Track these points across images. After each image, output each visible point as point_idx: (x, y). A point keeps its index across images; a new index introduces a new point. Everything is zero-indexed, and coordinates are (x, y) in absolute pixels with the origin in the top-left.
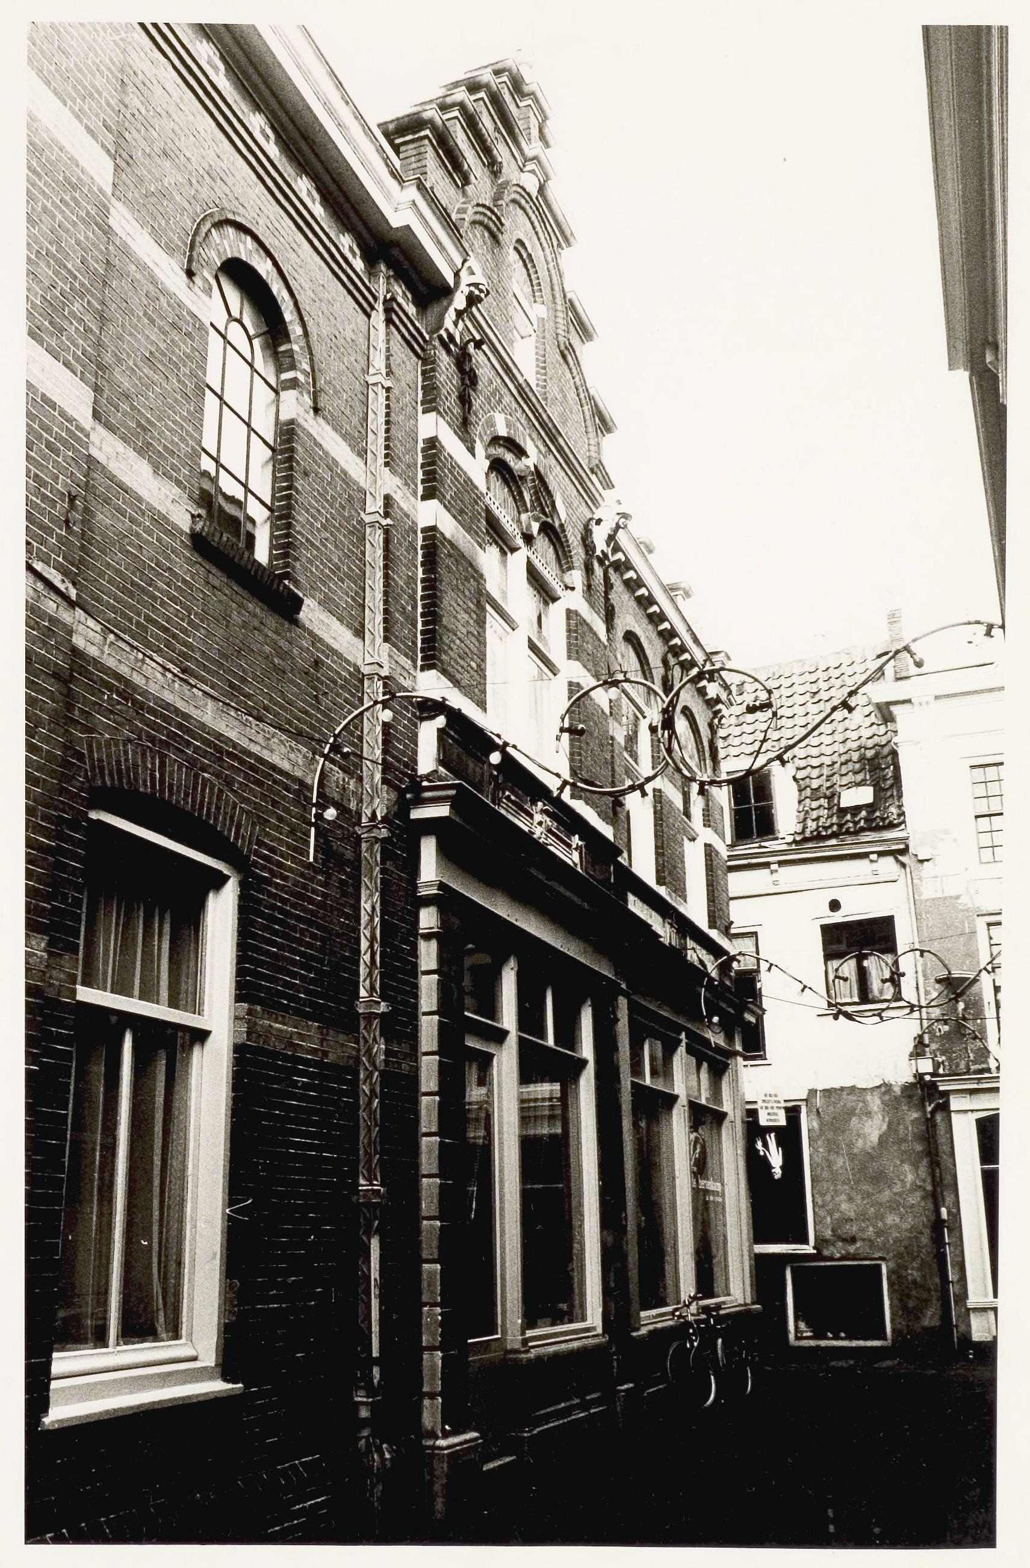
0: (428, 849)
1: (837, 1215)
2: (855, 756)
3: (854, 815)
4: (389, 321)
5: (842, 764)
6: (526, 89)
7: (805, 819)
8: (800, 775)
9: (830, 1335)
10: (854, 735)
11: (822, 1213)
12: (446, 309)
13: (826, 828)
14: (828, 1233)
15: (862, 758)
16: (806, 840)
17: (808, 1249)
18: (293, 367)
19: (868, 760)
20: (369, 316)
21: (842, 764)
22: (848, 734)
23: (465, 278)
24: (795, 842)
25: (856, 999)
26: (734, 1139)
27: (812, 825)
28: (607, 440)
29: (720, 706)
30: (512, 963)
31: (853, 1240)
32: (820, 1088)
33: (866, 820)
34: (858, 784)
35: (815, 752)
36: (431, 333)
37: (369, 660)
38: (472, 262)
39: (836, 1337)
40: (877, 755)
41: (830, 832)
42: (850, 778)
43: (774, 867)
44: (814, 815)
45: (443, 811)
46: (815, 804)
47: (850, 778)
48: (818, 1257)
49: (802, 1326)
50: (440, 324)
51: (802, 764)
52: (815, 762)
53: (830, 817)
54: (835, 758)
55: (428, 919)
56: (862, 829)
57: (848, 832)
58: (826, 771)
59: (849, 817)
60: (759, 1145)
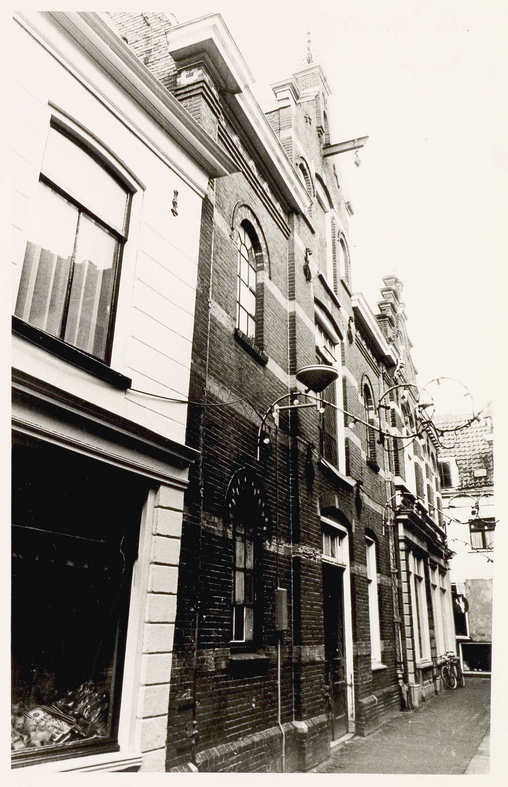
0: (401, 526)
1: (477, 626)
2: (478, 456)
3: (480, 480)
4: (384, 379)
5: (474, 459)
6: (399, 281)
7: (462, 481)
8: (459, 462)
9: (476, 670)
10: (477, 448)
11: (472, 624)
12: (394, 371)
13: (470, 485)
14: (474, 632)
15: (481, 458)
16: (463, 489)
17: (467, 638)
18: (372, 404)
19: (483, 458)
20: (378, 378)
21: (474, 459)
22: (475, 447)
23: (400, 362)
24: (459, 489)
25: (482, 547)
26: (448, 598)
27: (465, 483)
28: (416, 375)
29: (439, 448)
30: (411, 553)
31: (484, 635)
32: (470, 579)
33: (485, 482)
34: (480, 468)
35: (463, 454)
36: (391, 377)
37: (387, 477)
38: (401, 357)
39: (478, 671)
40: (486, 457)
41: (471, 486)
42: (477, 465)
43: (451, 498)
44: (465, 479)
45: (406, 517)
46: (465, 475)
47: (477, 465)
48: (471, 641)
49: (465, 666)
50: (393, 375)
51: (459, 458)
52: (464, 458)
53: (471, 480)
54: (471, 457)
55: (402, 545)
56: (483, 486)
57: (478, 487)
58: (468, 462)
59: (478, 481)
60: (457, 601)
